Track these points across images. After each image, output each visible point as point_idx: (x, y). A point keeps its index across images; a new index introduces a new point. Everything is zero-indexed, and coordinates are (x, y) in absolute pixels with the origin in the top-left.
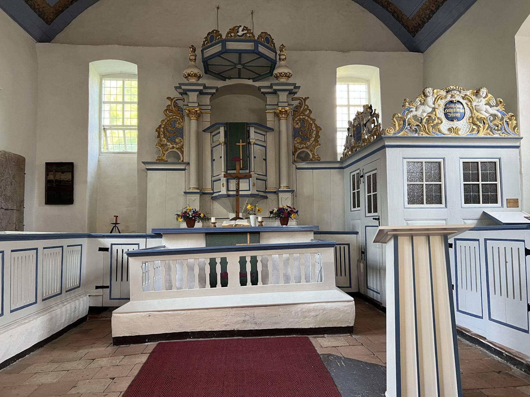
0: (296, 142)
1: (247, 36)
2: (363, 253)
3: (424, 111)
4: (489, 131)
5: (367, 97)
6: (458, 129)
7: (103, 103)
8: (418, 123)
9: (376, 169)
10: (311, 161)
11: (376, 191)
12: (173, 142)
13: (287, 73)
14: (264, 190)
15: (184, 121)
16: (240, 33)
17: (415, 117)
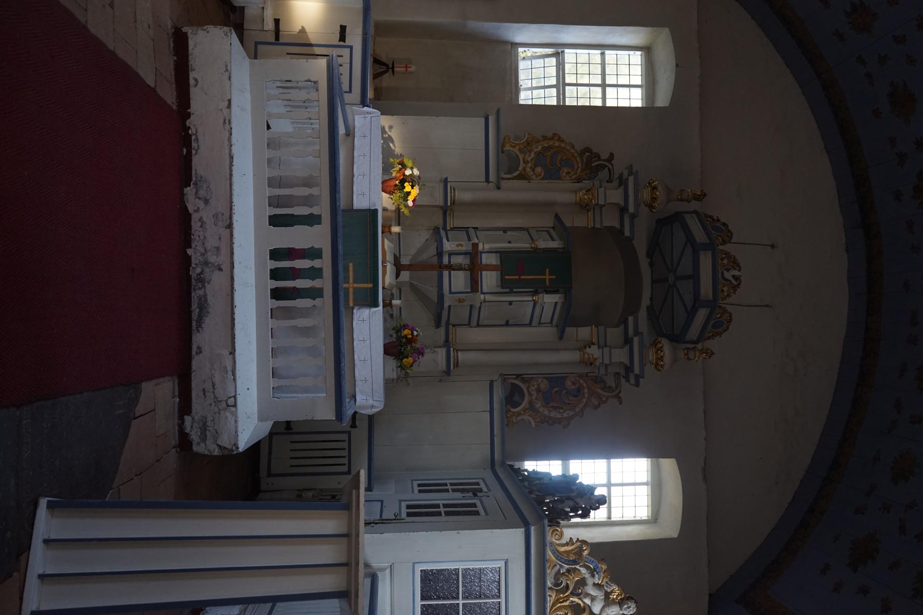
0: (540, 380)
1: (724, 287)
2: (334, 497)
5: (625, 519)
7: (603, 51)
8: (571, 588)
9: (487, 514)
11: (446, 515)
12: (536, 163)
13: (662, 361)
16: (728, 275)
17: (582, 582)
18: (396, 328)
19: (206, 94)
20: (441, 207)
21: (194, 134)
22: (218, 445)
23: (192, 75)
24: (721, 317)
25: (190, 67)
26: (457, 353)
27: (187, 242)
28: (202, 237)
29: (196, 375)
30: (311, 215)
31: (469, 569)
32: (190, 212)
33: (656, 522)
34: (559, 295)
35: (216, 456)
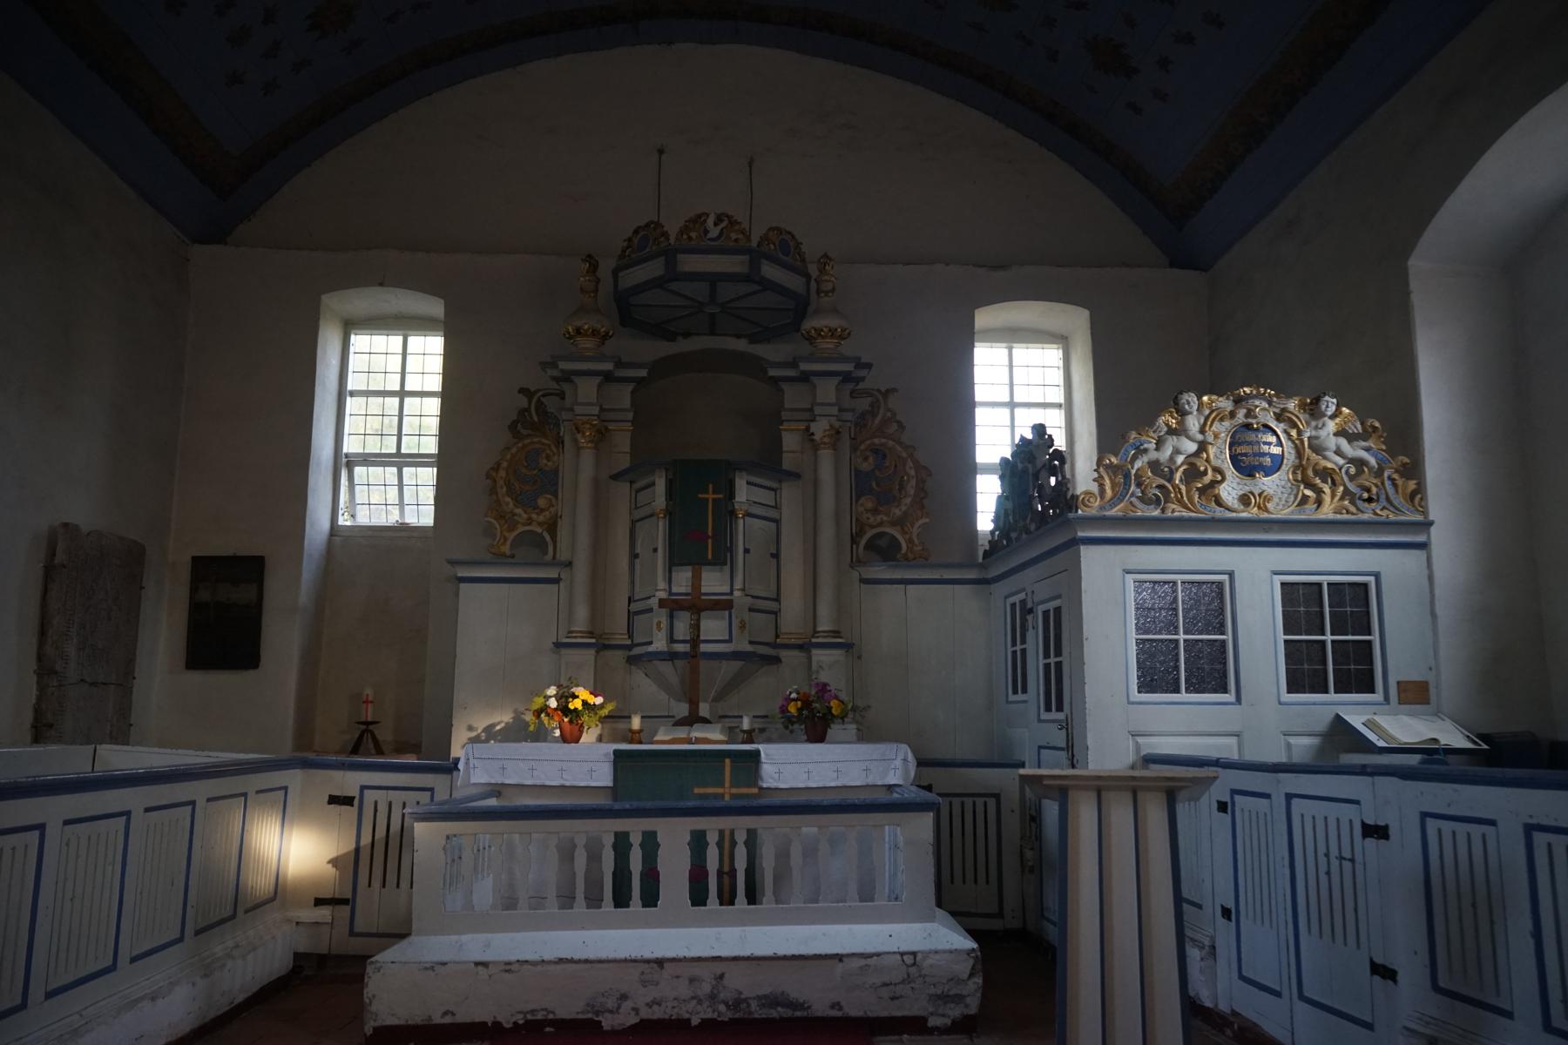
0: (861, 509)
2: (1033, 819)
3: (1177, 451)
4: (1346, 502)
6: (1265, 497)
7: (348, 393)
9: (1059, 597)
11: (1061, 655)
13: (836, 330)
14: (770, 638)
15: (561, 450)
16: (714, 233)
17: (1155, 466)
20: (597, 652)
21: (525, 1016)
24: (774, 244)
26: (819, 632)
27: (682, 1024)
28: (675, 1003)
30: (615, 847)
31: (1136, 624)
32: (638, 1021)
33: (1067, 338)
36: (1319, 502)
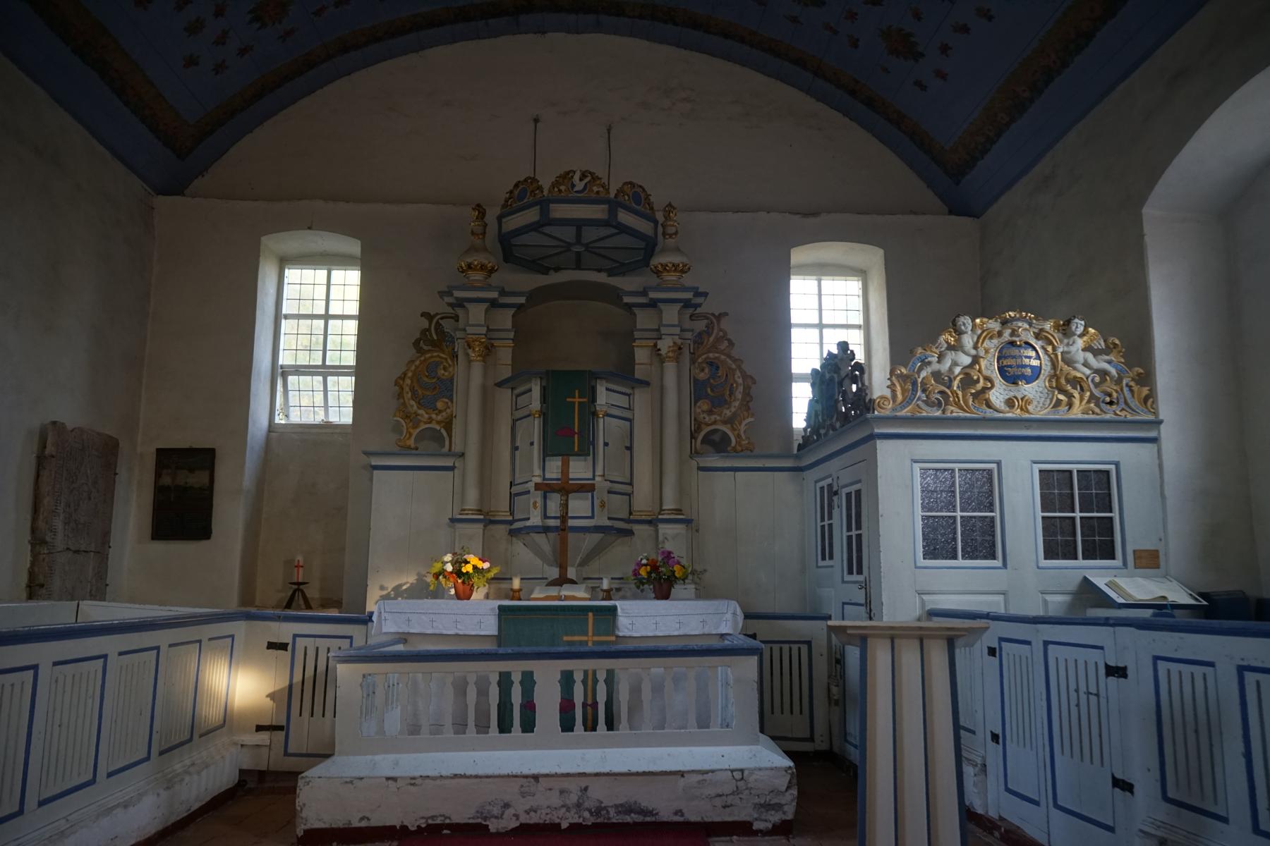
1: (593, 191)
2: (838, 661)
3: (955, 364)
4: (1092, 405)
9: (859, 481)
10: (738, 452)
13: (679, 265)
14: (624, 515)
15: (456, 363)
16: (579, 186)
17: (937, 375)
18: (638, 584)
19: (379, 807)
20: (485, 526)
22: (786, 790)
23: (356, 824)
24: (628, 195)
25: (346, 826)
26: (664, 510)
28: (549, 811)
29: (707, 817)
31: (922, 504)
34: (598, 386)
35: (798, 792)
36: (1070, 405)
